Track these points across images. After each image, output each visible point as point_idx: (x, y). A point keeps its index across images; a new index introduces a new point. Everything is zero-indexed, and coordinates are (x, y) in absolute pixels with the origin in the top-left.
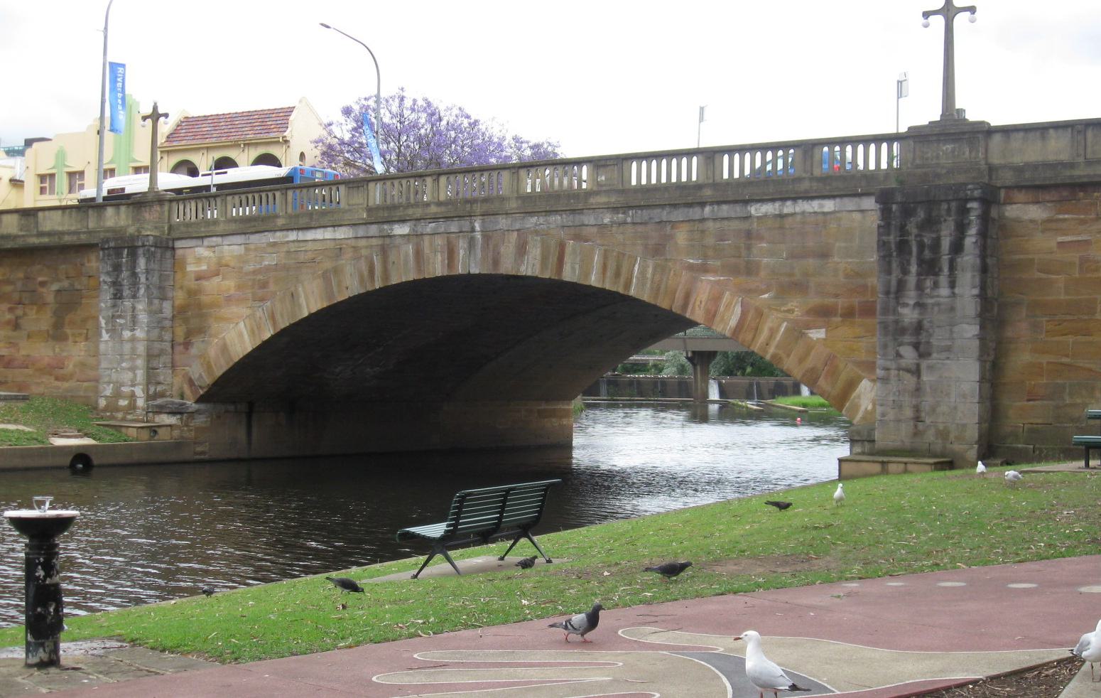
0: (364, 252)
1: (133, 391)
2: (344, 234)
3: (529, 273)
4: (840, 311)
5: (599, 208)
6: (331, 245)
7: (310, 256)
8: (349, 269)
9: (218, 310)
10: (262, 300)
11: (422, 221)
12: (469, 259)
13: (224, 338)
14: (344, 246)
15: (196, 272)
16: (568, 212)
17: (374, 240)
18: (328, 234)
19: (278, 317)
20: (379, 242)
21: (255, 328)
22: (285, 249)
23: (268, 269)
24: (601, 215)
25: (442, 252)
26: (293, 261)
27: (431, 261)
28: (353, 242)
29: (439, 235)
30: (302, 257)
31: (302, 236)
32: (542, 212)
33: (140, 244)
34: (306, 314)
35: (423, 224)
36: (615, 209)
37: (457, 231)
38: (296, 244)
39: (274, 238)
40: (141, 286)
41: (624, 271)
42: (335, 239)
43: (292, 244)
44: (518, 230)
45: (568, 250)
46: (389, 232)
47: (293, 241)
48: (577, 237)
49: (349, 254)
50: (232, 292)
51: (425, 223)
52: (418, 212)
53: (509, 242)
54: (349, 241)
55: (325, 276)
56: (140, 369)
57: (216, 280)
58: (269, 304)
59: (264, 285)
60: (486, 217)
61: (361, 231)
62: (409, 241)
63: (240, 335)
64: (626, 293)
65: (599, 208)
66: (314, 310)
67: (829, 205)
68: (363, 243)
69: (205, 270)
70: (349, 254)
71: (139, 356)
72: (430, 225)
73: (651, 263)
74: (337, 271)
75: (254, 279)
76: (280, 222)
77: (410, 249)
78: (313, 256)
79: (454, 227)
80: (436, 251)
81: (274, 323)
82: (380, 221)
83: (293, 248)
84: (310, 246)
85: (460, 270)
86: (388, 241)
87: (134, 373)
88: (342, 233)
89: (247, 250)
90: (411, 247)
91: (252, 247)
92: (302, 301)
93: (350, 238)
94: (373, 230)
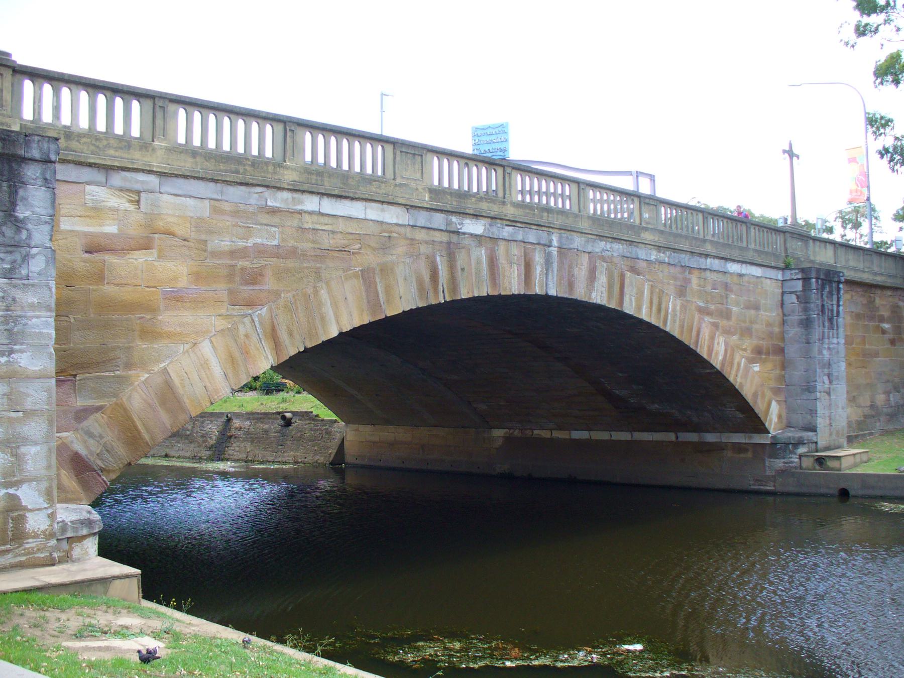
0: (423, 249)
1: (14, 498)
2: (397, 217)
3: (599, 302)
4: (764, 351)
5: (650, 244)
6: (373, 229)
7: (339, 241)
8: (401, 271)
9: (148, 316)
10: (251, 304)
11: (498, 221)
12: (547, 278)
13: (165, 371)
14: (395, 235)
15: (86, 234)
16: (628, 243)
17: (437, 234)
18: (373, 212)
19: (283, 335)
20: (444, 237)
21: (237, 354)
22: (296, 223)
23: (261, 251)
24: (649, 251)
25: (518, 265)
26: (311, 245)
27: (507, 274)
28: (408, 232)
29: (515, 243)
30: (327, 242)
31: (329, 206)
32: (609, 237)
33: (35, 153)
34: (334, 333)
35: (499, 225)
36: (659, 248)
37: (535, 242)
38: (315, 218)
39: (275, 200)
40: (34, 251)
41: (663, 306)
42: (382, 222)
43: (307, 217)
44: (589, 253)
45: (627, 281)
46: (459, 227)
47: (311, 213)
48: (633, 270)
49: (401, 249)
50: (183, 283)
51: (502, 224)
52: (495, 209)
53: (582, 265)
54: (402, 230)
55: (367, 276)
56: (36, 443)
57: (139, 258)
58: (264, 311)
59: (253, 278)
60: (562, 231)
61: (422, 219)
62: (480, 244)
63: (204, 365)
64: (664, 329)
65: (650, 244)
66: (347, 328)
67: (757, 271)
68: (421, 235)
69: (113, 235)
70: (401, 249)
71: (29, 414)
72: (507, 228)
73: (679, 302)
74: (386, 270)
75: (232, 266)
76: (289, 177)
77: (482, 253)
78: (346, 242)
79: (532, 236)
80: (511, 263)
81: (277, 345)
82: (450, 210)
83: (309, 222)
84: (341, 226)
85: (538, 290)
86: (454, 238)
87: (15, 455)
88: (392, 216)
89: (216, 211)
90: (483, 252)
91: (226, 207)
92: (329, 311)
93: (404, 226)
94: (439, 220)
